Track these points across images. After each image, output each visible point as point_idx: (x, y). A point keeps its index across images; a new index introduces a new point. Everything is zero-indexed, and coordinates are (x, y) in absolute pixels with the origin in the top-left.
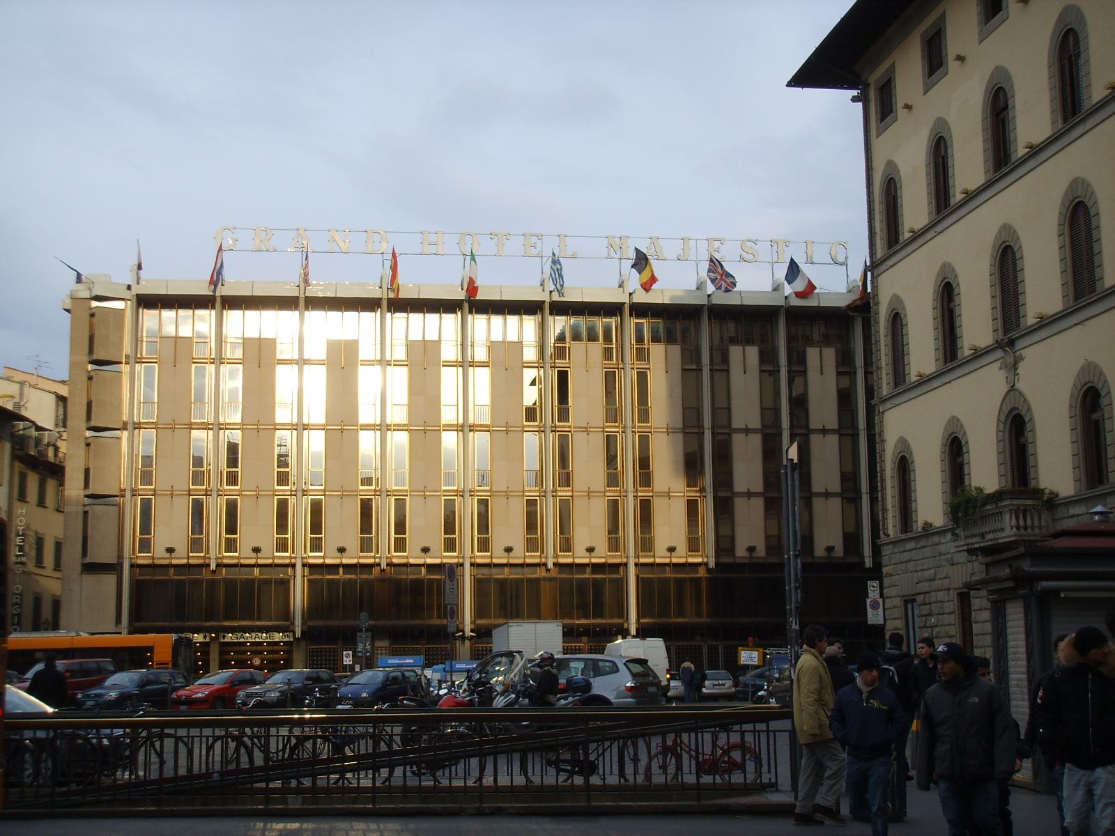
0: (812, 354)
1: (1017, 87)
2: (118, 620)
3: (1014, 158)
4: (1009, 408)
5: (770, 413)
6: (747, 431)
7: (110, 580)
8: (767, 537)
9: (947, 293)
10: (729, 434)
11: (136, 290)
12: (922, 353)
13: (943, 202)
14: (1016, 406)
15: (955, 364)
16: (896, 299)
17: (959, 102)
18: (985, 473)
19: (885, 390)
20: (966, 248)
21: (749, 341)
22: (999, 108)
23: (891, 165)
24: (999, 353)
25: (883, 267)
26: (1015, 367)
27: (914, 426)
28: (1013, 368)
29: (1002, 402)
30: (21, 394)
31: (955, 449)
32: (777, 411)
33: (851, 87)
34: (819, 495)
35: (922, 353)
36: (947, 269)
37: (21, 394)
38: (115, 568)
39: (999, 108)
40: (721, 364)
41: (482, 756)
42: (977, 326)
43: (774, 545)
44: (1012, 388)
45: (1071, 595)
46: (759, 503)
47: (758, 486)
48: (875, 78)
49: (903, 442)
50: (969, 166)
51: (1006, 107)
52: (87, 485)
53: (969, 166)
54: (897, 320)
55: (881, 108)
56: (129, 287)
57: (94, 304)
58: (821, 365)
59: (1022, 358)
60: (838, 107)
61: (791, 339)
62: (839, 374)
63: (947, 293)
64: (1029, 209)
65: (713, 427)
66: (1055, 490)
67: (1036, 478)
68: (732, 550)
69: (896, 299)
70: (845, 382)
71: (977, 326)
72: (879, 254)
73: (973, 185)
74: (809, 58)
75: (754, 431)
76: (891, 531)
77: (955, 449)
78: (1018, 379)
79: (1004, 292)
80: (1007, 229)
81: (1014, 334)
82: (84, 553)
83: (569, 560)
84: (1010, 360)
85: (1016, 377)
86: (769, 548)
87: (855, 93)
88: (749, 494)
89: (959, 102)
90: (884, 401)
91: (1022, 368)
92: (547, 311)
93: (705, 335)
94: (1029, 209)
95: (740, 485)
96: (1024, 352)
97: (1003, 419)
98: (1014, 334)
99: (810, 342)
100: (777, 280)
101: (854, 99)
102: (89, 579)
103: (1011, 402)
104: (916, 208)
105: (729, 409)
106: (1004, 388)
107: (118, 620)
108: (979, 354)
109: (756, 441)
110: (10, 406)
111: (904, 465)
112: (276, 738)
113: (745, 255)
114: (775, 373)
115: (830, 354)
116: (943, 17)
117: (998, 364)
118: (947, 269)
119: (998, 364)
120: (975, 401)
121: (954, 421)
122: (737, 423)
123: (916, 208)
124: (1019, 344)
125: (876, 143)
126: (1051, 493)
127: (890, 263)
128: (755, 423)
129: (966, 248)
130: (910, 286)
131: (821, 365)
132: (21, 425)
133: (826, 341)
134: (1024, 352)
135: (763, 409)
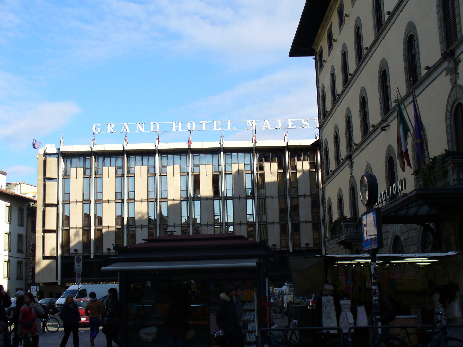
4: (453, 100)
8: (314, 239)
14: (458, 97)
25: (327, 182)
29: (451, 92)
46: (310, 226)
59: (460, 61)
60: (309, 62)
65: (290, 195)
78: (458, 77)
79: (355, 207)
81: (452, 47)
85: (457, 76)
86: (315, 244)
88: (306, 222)
97: (449, 109)
101: (313, 58)
103: (297, 338)
105: (297, 188)
106: (449, 86)
112: (56, 177)
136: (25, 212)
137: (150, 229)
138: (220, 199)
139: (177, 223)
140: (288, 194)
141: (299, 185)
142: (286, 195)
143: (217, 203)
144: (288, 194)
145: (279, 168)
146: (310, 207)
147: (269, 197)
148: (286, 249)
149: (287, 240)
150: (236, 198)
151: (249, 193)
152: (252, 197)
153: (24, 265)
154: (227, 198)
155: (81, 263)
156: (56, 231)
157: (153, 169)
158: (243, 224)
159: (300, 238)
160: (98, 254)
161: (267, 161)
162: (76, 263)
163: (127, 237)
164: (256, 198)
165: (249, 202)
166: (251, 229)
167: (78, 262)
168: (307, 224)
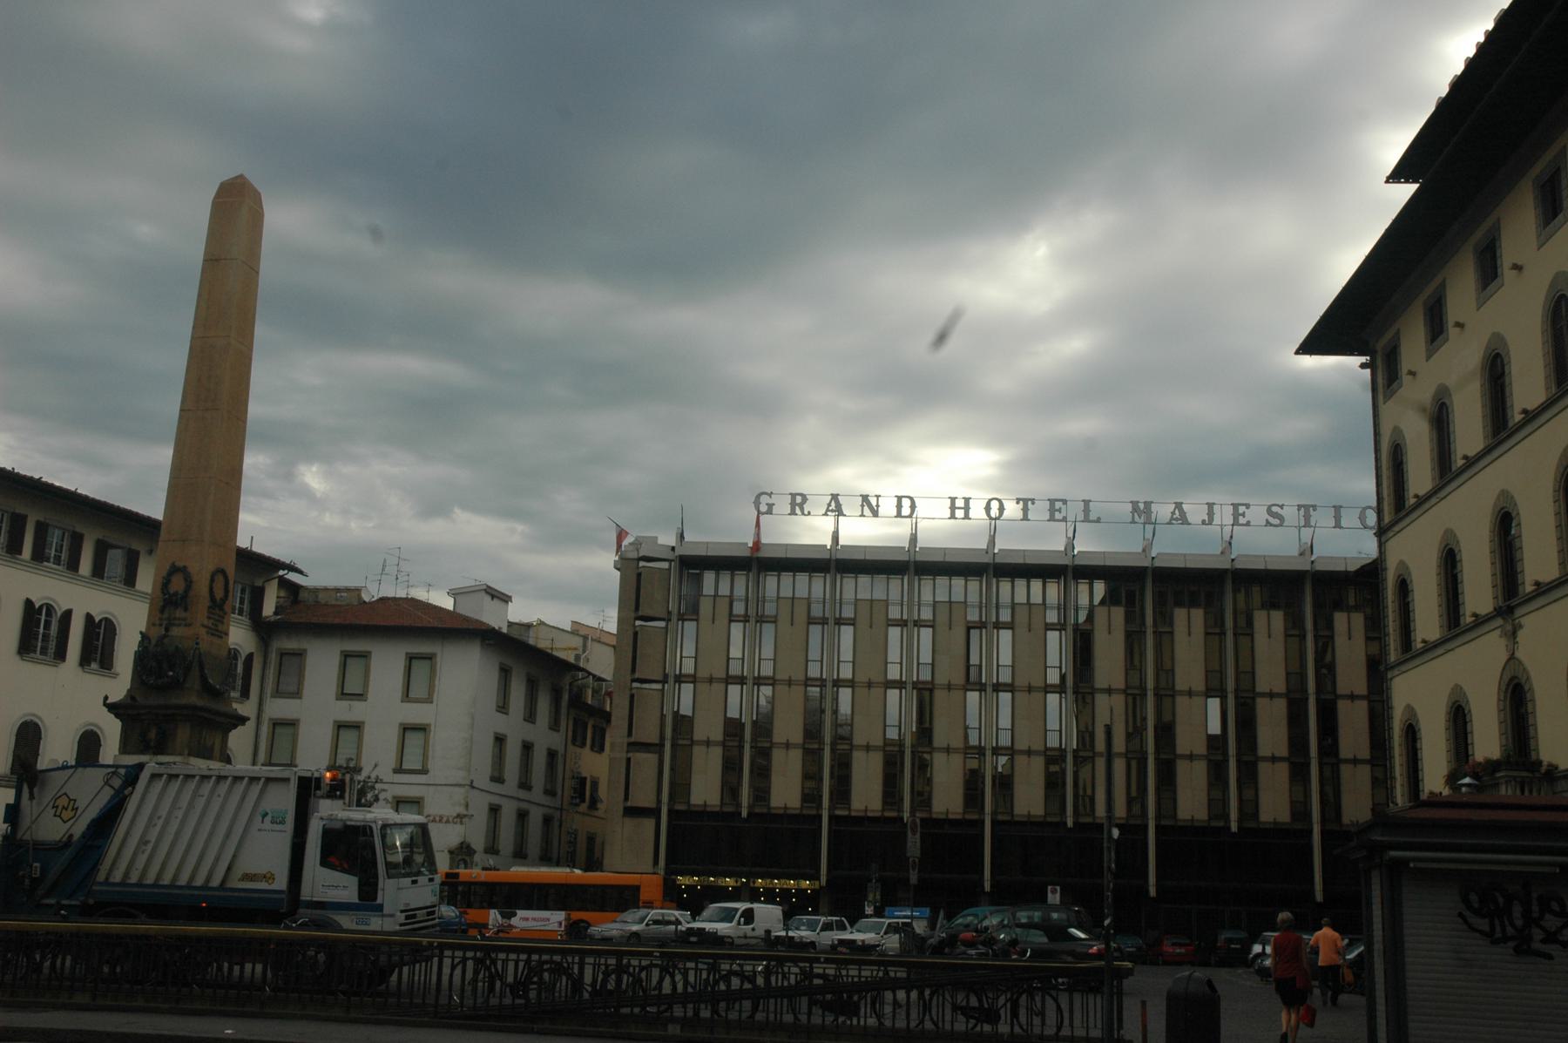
0: (1340, 619)
1: (1512, 353)
2: (656, 862)
3: (1511, 424)
5: (1295, 678)
6: (1271, 695)
7: (648, 824)
9: (1450, 560)
10: (1253, 699)
11: (679, 552)
12: (1428, 622)
13: (1447, 470)
15: (1458, 630)
16: (1402, 564)
17: (1454, 368)
18: (1488, 743)
19: (1393, 658)
20: (1465, 514)
21: (1193, 603)
22: (1495, 371)
23: (1397, 431)
24: (1499, 622)
25: (1390, 534)
26: (1514, 634)
27: (1419, 693)
28: (1512, 635)
30: (585, 646)
31: (1459, 717)
32: (1302, 676)
33: (1360, 354)
34: (1347, 761)
35: (1428, 622)
36: (1449, 534)
37: (585, 646)
38: (654, 813)
39: (1495, 371)
40: (1246, 630)
41: (776, 997)
42: (1479, 595)
43: (1300, 811)
44: (1512, 657)
45: (1420, 865)
47: (1283, 751)
48: (1381, 344)
49: (1410, 710)
50: (1469, 433)
51: (1503, 373)
52: (630, 734)
53: (1469, 433)
54: (1404, 587)
55: (1387, 375)
56: (673, 549)
57: (642, 564)
58: (1349, 630)
59: (1521, 627)
61: (1317, 606)
62: (1368, 639)
63: (1450, 560)
64: (1527, 474)
66: (1554, 762)
67: (1537, 750)
68: (1256, 814)
69: (1402, 564)
70: (1375, 649)
71: (1479, 595)
72: (1387, 519)
73: (1472, 452)
74: (191, 348)
75: (1279, 695)
76: (1399, 800)
77: (1459, 717)
80: (1504, 494)
82: (626, 798)
83: (845, 813)
84: (1509, 627)
87: (1363, 359)
89: (1454, 368)
90: (1392, 668)
91: (1521, 634)
92: (1070, 575)
93: (1229, 601)
94: (1527, 474)
95: (1264, 749)
96: (1523, 621)
98: (1514, 602)
99: (1339, 605)
100: (637, 544)
101: (1363, 366)
102: (630, 823)
104: (1420, 477)
105: (1253, 673)
106: (1504, 657)
107: (656, 862)
108: (1480, 621)
109: (1281, 705)
110: (572, 660)
111: (1411, 733)
113: (1272, 520)
114: (1303, 637)
115: (1358, 619)
116: (1443, 285)
117: (1498, 632)
118: (1449, 534)
119: (1498, 632)
120: (1475, 668)
121: (1457, 689)
122: (1262, 686)
123: (1420, 477)
124: (1519, 612)
125: (1384, 409)
126: (1550, 765)
127: (1396, 529)
128: (1280, 686)
129: (1465, 514)
130: (1415, 552)
131: (1349, 630)
132: (580, 675)
133: (1270, 605)
134: (1523, 621)
135: (1288, 674)
136: (566, 697)
137: (807, 752)
138: (981, 688)
139: (1035, 747)
140: (1150, 684)
141: (1257, 667)
142: (1143, 689)
143: (973, 697)
144: (1150, 684)
145: (1128, 618)
146: (1284, 722)
147: (1182, 693)
148: (1222, 824)
149: (1225, 802)
150: (1038, 689)
151: (1053, 677)
152: (1061, 689)
153: (556, 824)
154: (998, 688)
155: (918, 835)
156: (657, 748)
157: (742, 605)
158: (1037, 753)
159: (1257, 795)
160: (757, 810)
161: (1179, 604)
162: (909, 834)
163: (752, 772)
164: (1070, 691)
165: (1053, 699)
166: (973, 764)
167: (914, 833)
168: (1359, 767)
